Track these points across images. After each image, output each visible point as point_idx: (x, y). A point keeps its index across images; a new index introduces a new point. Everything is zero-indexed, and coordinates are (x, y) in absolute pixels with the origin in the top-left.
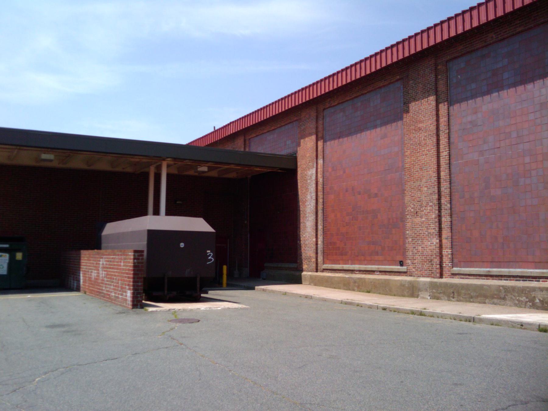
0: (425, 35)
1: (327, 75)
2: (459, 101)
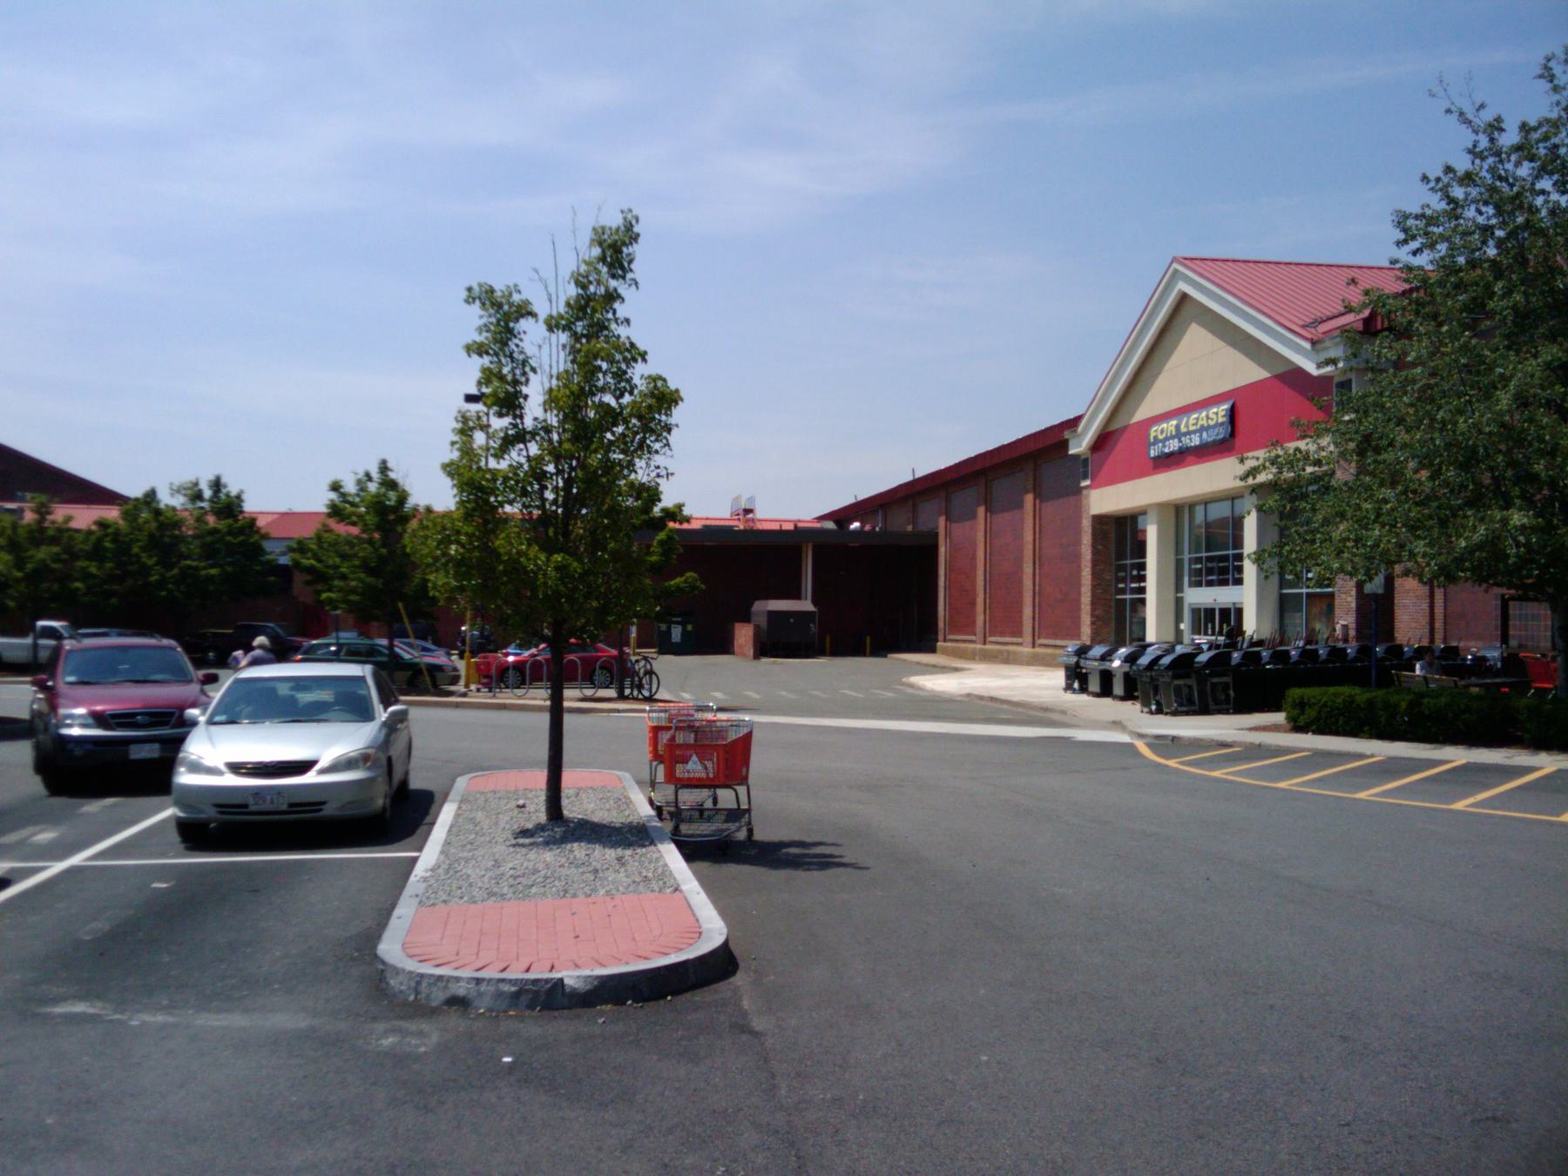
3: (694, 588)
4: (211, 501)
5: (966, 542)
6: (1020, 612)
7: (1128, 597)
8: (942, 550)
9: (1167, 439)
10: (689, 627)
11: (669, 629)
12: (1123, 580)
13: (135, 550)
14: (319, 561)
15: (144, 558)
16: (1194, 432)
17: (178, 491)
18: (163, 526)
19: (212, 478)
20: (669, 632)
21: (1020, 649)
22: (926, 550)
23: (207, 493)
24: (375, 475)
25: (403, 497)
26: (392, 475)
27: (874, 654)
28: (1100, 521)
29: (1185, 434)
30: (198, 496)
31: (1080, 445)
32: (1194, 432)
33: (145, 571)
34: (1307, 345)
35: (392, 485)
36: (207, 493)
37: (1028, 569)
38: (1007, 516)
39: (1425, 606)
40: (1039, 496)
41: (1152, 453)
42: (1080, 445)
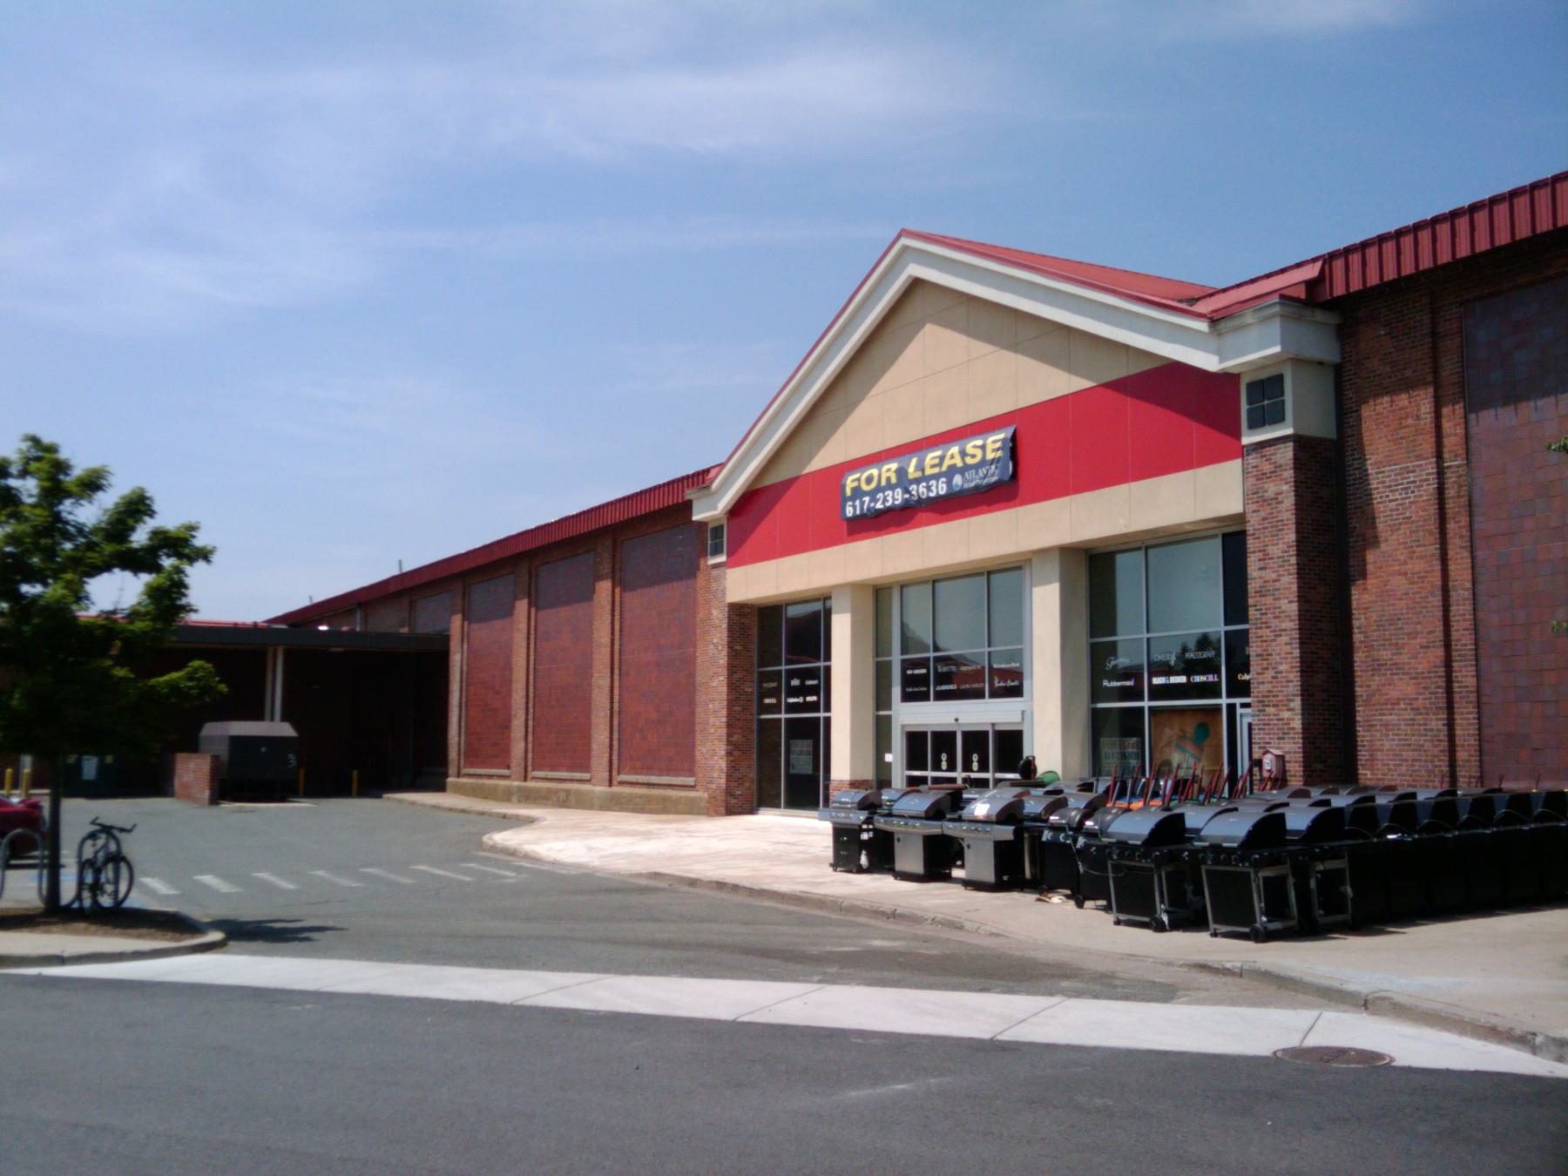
0: (1389, 247)
1: (1486, 196)
2: (634, 589)
5: (497, 653)
6: (587, 738)
7: (783, 716)
9: (879, 489)
11: (79, 761)
12: (775, 693)
16: (936, 477)
20: (78, 767)
21: (586, 787)
22: (434, 658)
28: (739, 611)
29: (917, 481)
31: (711, 509)
32: (936, 477)
34: (1202, 326)
37: (601, 681)
38: (564, 612)
39: (1438, 723)
40: (619, 582)
41: (849, 512)
42: (711, 509)
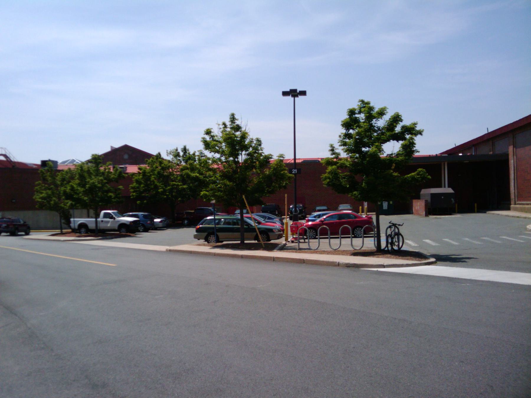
3: (424, 178)
4: (183, 156)
8: (512, 162)
10: (391, 203)
11: (382, 204)
13: (152, 179)
14: (201, 174)
15: (156, 183)
17: (169, 154)
18: (163, 169)
19: (183, 147)
22: (502, 163)
23: (181, 154)
24: (228, 124)
25: (244, 136)
26: (237, 122)
27: (479, 212)
30: (177, 155)
33: (156, 187)
35: (238, 128)
36: (181, 154)
